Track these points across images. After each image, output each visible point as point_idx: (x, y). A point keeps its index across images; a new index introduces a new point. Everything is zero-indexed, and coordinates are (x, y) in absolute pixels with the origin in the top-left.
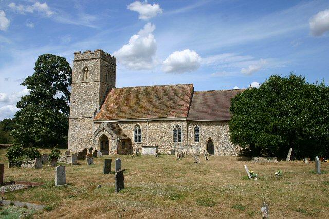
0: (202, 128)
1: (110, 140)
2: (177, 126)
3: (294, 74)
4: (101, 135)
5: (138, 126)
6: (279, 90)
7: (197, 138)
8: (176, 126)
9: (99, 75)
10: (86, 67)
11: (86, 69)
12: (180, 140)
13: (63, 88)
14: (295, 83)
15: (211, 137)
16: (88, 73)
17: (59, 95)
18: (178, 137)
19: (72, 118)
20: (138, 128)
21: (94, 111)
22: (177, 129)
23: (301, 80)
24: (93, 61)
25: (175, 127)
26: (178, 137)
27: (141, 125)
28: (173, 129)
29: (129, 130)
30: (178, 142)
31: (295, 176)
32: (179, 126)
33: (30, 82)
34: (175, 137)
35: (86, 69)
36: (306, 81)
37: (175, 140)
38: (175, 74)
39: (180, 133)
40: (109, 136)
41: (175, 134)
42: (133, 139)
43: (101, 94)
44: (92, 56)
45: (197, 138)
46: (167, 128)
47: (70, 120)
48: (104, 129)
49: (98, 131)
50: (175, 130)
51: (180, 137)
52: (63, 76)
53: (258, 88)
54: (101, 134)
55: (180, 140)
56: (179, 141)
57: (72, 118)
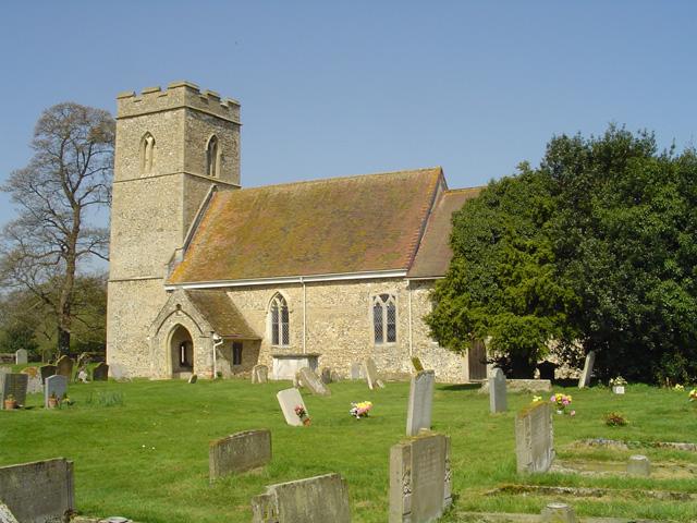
1: (194, 340)
2: (385, 297)
3: (619, 128)
5: (280, 297)
6: (598, 173)
9: (182, 155)
10: (149, 134)
11: (150, 140)
12: (392, 339)
14: (617, 159)
16: (155, 150)
18: (386, 330)
21: (166, 260)
23: (642, 150)
24: (167, 115)
25: (379, 299)
26: (386, 330)
28: (372, 304)
29: (256, 311)
30: (386, 344)
31: (561, 425)
32: (388, 296)
33: (23, 183)
34: (378, 331)
35: (150, 140)
36: (661, 148)
37: (379, 337)
39: (391, 313)
40: (192, 330)
41: (378, 319)
42: (268, 336)
43: (188, 210)
49: (164, 316)
50: (378, 308)
51: (392, 327)
54: (172, 323)
55: (392, 339)
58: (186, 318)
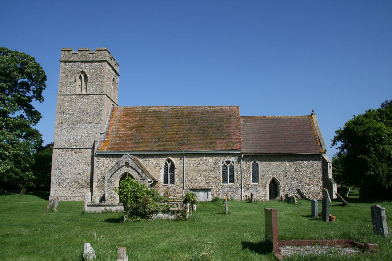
0: (262, 165)
2: (228, 162)
4: (122, 173)
5: (169, 161)
7: (255, 178)
8: (226, 162)
12: (232, 181)
13: (25, 104)
15: (275, 176)
17: (17, 114)
19: (56, 149)
20: (169, 165)
22: (228, 166)
26: (229, 176)
27: (174, 160)
28: (222, 165)
32: (230, 162)
37: (225, 180)
38: (386, 102)
44: (93, 57)
45: (255, 178)
46: (213, 165)
47: (54, 150)
48: (127, 164)
49: (116, 168)
50: (225, 167)
51: (232, 176)
52: (23, 84)
53: (45, 81)
55: (232, 181)
56: (230, 182)
57: (56, 149)
58: (131, 170)
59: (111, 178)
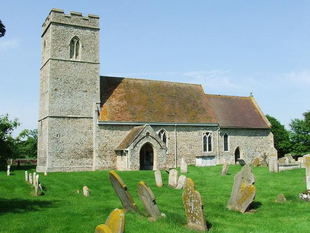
18: (207, 144)
25: (205, 134)
39: (210, 138)
45: (226, 149)
50: (205, 137)
51: (210, 146)
58: (152, 139)
59: (134, 147)
